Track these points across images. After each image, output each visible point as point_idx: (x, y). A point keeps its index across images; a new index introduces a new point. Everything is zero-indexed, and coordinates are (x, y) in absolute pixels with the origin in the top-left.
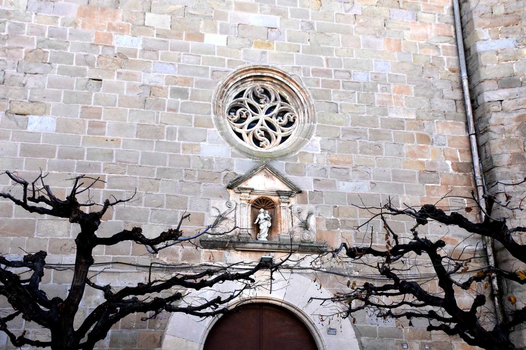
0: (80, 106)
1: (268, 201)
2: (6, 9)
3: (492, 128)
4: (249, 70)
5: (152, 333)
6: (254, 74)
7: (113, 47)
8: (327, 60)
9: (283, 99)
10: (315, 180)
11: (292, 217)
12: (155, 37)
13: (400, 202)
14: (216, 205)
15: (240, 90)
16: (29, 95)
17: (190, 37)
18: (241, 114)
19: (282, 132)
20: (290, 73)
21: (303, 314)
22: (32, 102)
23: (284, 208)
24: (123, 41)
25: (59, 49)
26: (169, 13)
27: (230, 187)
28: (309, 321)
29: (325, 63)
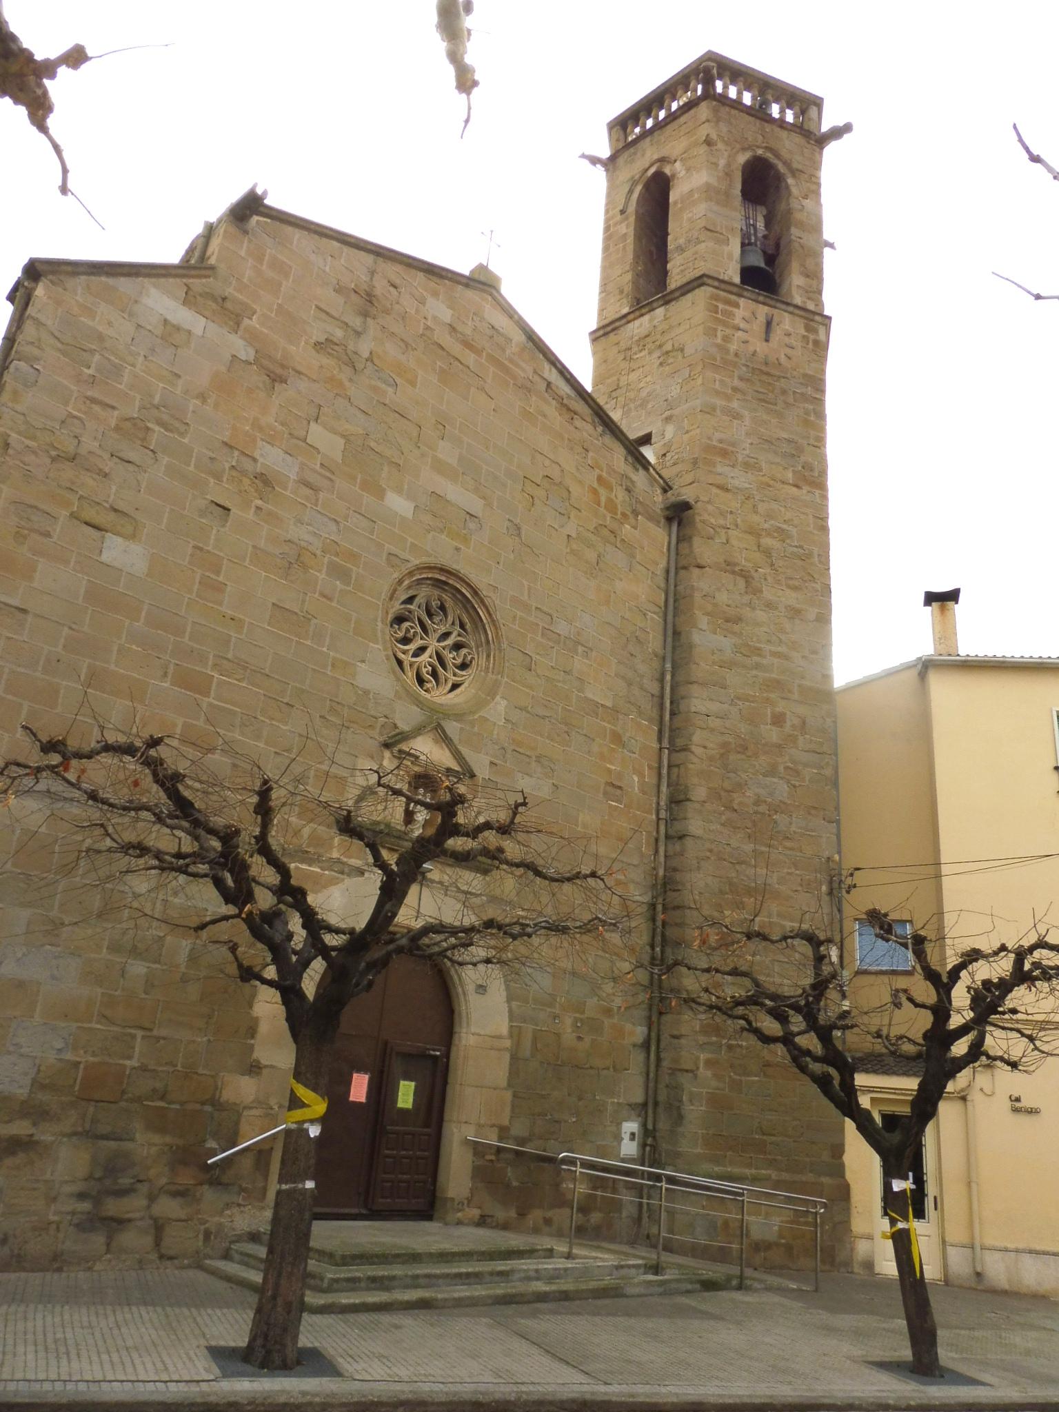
0: (192, 543)
2: (100, 329)
3: (693, 748)
4: (435, 568)
6: (437, 576)
7: (255, 460)
8: (529, 588)
9: (462, 626)
10: (491, 763)
12: (318, 467)
15: (411, 593)
16: (112, 497)
17: (365, 486)
18: (407, 631)
19: (455, 675)
20: (484, 592)
22: (116, 510)
24: (271, 457)
25: (171, 431)
26: (343, 436)
27: (387, 746)
29: (526, 593)
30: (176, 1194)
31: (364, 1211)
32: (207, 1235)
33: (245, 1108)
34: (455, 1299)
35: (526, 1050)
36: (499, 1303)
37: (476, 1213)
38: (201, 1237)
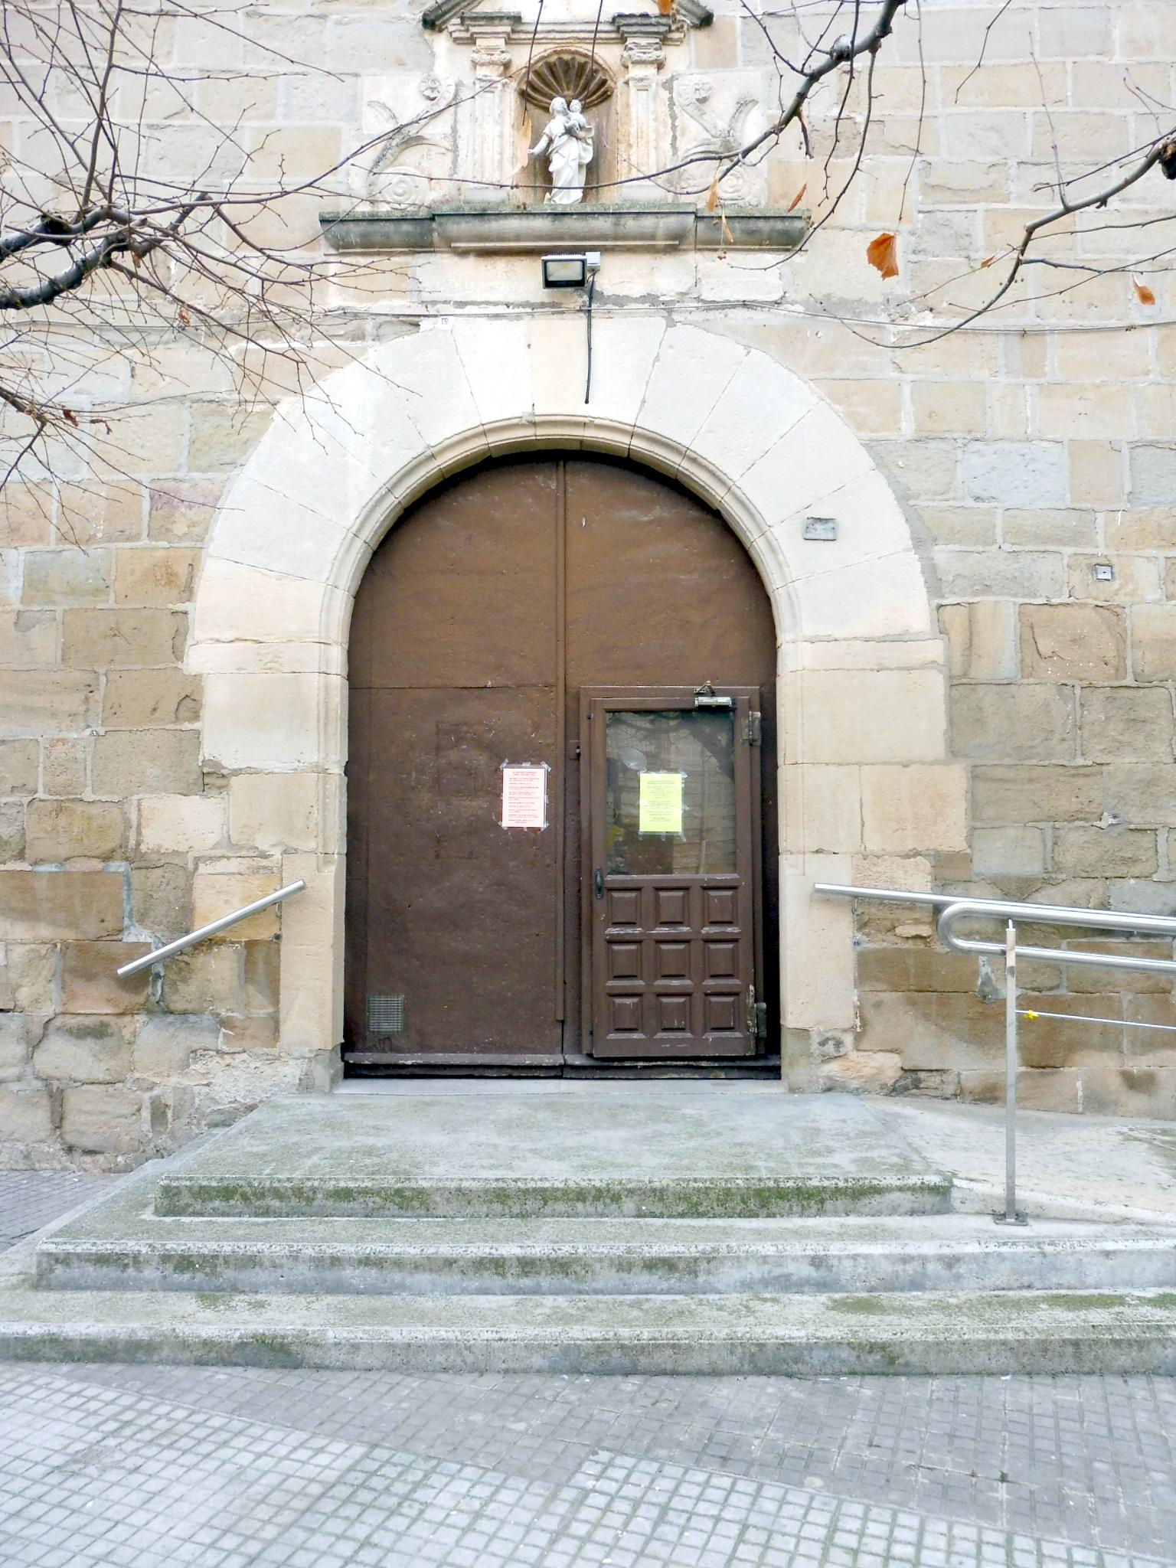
1: (582, 66)
5: (161, 553)
11: (673, 117)
13: (1116, 33)
14: (385, 95)
21: (713, 474)
23: (643, 85)
27: (431, 23)
28: (735, 495)
30: (81, 1033)
31: (577, 1060)
32: (159, 1112)
33: (197, 860)
34: (391, 1347)
35: (1001, 651)
36: (577, 1371)
37: (888, 1065)
38: (146, 1114)
